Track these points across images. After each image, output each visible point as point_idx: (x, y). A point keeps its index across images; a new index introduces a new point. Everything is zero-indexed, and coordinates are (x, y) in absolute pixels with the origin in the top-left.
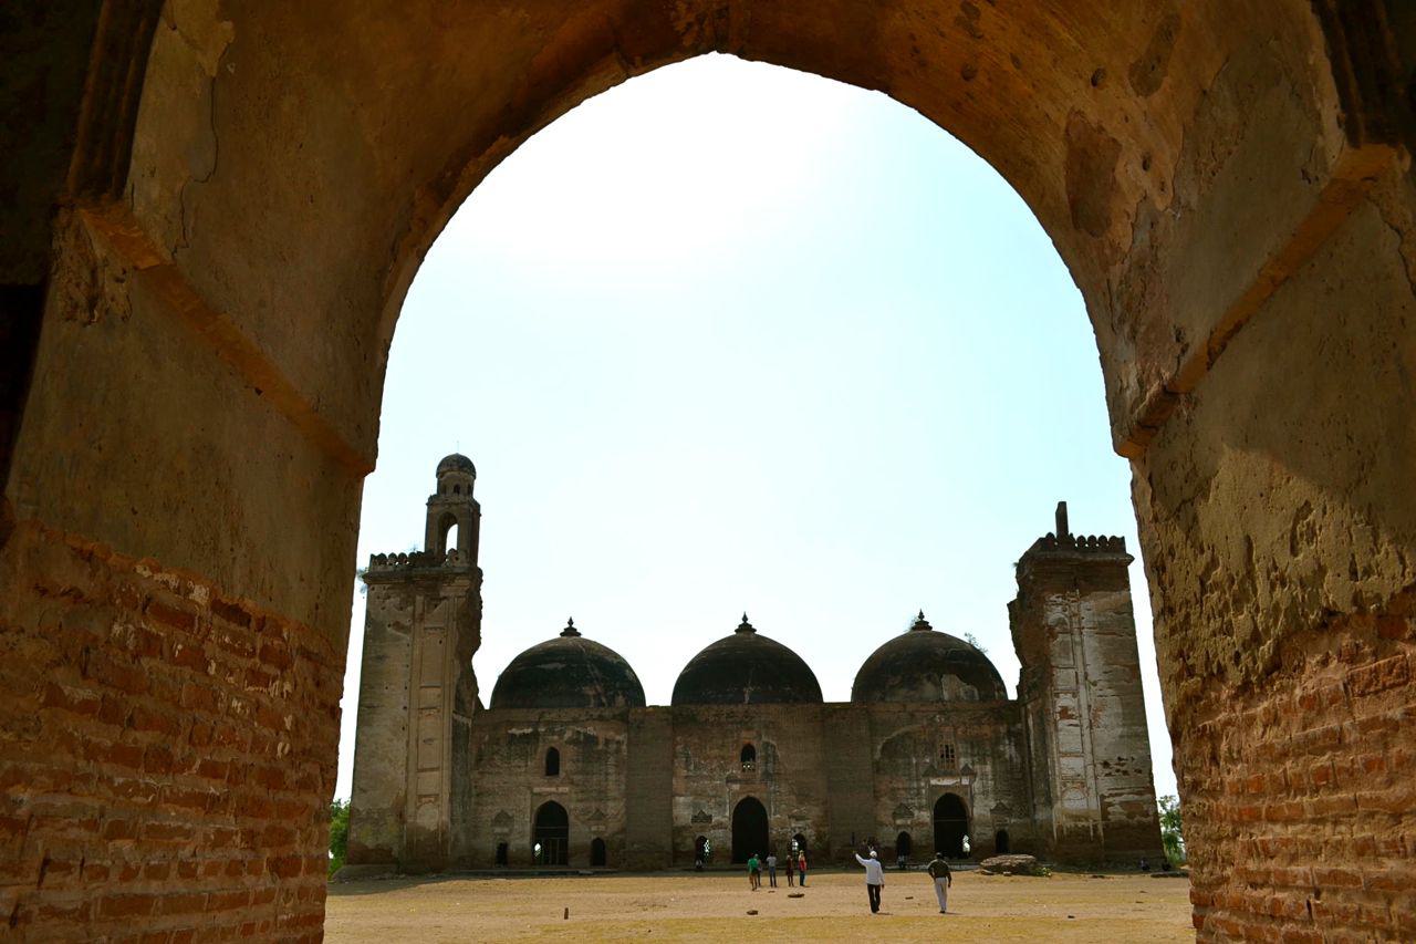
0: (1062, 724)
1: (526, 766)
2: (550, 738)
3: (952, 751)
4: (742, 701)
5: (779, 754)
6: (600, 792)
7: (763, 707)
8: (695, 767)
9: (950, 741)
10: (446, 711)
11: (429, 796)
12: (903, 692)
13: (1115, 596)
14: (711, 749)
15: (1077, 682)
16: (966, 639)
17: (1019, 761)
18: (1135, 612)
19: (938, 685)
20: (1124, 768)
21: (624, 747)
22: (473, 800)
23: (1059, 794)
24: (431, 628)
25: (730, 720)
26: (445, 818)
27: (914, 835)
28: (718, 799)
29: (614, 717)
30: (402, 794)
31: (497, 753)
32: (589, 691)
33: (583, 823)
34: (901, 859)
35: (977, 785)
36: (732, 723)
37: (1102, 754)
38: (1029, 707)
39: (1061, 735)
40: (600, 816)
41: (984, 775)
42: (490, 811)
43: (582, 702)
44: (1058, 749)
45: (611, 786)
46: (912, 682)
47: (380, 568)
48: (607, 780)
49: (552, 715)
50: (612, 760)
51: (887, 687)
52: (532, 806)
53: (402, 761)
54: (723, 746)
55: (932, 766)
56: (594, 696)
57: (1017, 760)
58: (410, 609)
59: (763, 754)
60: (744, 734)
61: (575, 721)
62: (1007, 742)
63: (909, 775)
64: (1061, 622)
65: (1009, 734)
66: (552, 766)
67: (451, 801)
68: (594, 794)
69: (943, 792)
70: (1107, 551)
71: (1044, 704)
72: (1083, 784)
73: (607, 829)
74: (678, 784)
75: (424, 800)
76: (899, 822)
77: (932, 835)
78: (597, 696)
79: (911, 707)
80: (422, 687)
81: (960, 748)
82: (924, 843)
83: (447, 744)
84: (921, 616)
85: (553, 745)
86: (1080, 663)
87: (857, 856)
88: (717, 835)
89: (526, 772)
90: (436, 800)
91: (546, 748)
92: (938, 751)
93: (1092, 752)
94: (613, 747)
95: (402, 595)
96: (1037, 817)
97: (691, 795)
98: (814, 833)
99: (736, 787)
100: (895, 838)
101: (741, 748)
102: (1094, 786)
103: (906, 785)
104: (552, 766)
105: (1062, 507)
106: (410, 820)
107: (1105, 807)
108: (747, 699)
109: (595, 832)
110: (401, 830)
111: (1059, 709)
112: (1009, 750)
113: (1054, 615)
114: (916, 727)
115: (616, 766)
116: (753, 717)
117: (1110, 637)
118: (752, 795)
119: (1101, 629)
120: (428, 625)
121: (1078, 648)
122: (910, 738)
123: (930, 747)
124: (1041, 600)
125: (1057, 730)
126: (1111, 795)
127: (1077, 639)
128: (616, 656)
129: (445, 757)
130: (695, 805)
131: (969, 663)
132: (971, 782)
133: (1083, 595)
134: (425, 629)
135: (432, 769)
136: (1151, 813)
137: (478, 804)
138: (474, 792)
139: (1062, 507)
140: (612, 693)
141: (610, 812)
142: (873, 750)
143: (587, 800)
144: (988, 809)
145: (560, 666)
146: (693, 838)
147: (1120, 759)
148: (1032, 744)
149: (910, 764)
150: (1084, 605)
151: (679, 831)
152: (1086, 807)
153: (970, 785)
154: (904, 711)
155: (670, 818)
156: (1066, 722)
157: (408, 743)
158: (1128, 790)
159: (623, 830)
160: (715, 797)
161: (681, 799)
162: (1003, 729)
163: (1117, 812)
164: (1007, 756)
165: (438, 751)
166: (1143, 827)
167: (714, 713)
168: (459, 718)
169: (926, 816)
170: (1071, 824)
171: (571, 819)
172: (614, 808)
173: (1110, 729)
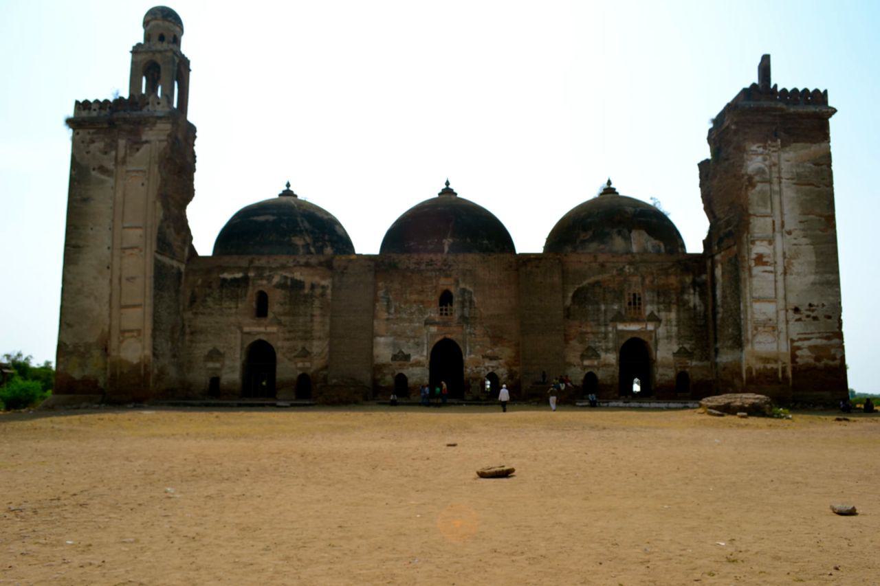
0: (757, 270)
1: (237, 307)
2: (260, 282)
3: (639, 299)
4: (442, 251)
5: (475, 299)
6: (306, 332)
7: (461, 257)
8: (395, 311)
9: (638, 290)
10: (148, 250)
11: (132, 331)
12: (593, 246)
13: (814, 149)
14: (411, 293)
15: (774, 230)
16: (651, 202)
17: (702, 308)
18: (833, 164)
19: (627, 239)
20: (813, 314)
21: (329, 291)
22: (187, 338)
23: (750, 337)
24: (134, 171)
25: (430, 267)
26: (148, 352)
27: (600, 374)
28: (417, 340)
29: (320, 264)
30: (107, 329)
31: (209, 295)
32: (298, 241)
33: (290, 360)
34: (592, 397)
35: (662, 330)
36: (432, 270)
37: (793, 301)
38: (718, 257)
39: (755, 282)
40: (305, 354)
41: (669, 321)
42: (202, 348)
43: (292, 249)
44: (751, 294)
45: (317, 327)
46: (601, 237)
47: (84, 114)
48: (312, 321)
49: (262, 262)
50: (317, 303)
51: (578, 242)
52: (242, 344)
53: (106, 299)
54: (422, 291)
55: (619, 313)
56: (303, 246)
57: (700, 309)
58: (113, 153)
59: (460, 299)
60: (443, 281)
61: (283, 267)
62: (692, 291)
63: (598, 320)
64: (760, 172)
65: (695, 284)
66: (261, 309)
67: (154, 337)
68: (300, 334)
69: (629, 337)
70: (808, 103)
71: (739, 251)
72: (774, 328)
73: (313, 365)
74: (379, 326)
75: (127, 335)
76: (586, 363)
77: (617, 374)
78: (307, 246)
79: (601, 258)
80: (124, 228)
81: (648, 296)
82: (609, 382)
83: (150, 282)
84: (609, 183)
85: (261, 288)
86: (777, 212)
87: (791, 384)
88: (415, 372)
89: (236, 313)
90: (139, 335)
91: (256, 291)
92: (627, 300)
93: (785, 298)
94: (318, 291)
95: (106, 140)
96: (718, 360)
97: (391, 336)
98: (506, 372)
99: (434, 329)
100: (582, 378)
101: (439, 293)
102: (784, 330)
103: (595, 329)
104: (261, 309)
105: (766, 60)
106: (114, 354)
107: (794, 349)
108: (446, 249)
109: (300, 369)
110: (106, 363)
111: (753, 256)
112: (693, 299)
113: (754, 163)
114: (606, 276)
115: (321, 308)
116: (450, 266)
117: (808, 187)
118: (449, 336)
119: (800, 180)
120: (130, 168)
121: (776, 199)
122: (601, 287)
123: (618, 295)
124: (741, 149)
125: (751, 276)
126: (800, 339)
127: (776, 188)
128: (327, 214)
129: (148, 294)
130: (394, 345)
131: (657, 225)
132: (656, 328)
133: (784, 145)
134: (127, 171)
135: (134, 306)
136: (838, 357)
137: (192, 341)
138: (188, 330)
139: (766, 60)
140: (320, 244)
141: (315, 350)
142: (564, 297)
143: (294, 339)
144: (671, 352)
145: (271, 218)
146: (392, 374)
147: (810, 305)
148: (719, 293)
149: (599, 310)
150: (784, 156)
151: (378, 368)
152: (775, 349)
153: (655, 331)
154: (595, 262)
155: (371, 356)
156: (761, 268)
157: (111, 281)
158: (818, 335)
159: (326, 367)
160: (414, 338)
161: (382, 340)
162: (688, 280)
163: (805, 356)
164: (691, 305)
165: (140, 289)
166: (828, 369)
167: (414, 261)
168: (167, 260)
169: (612, 358)
170: (759, 365)
171: (279, 356)
172: (318, 347)
173: (803, 277)
